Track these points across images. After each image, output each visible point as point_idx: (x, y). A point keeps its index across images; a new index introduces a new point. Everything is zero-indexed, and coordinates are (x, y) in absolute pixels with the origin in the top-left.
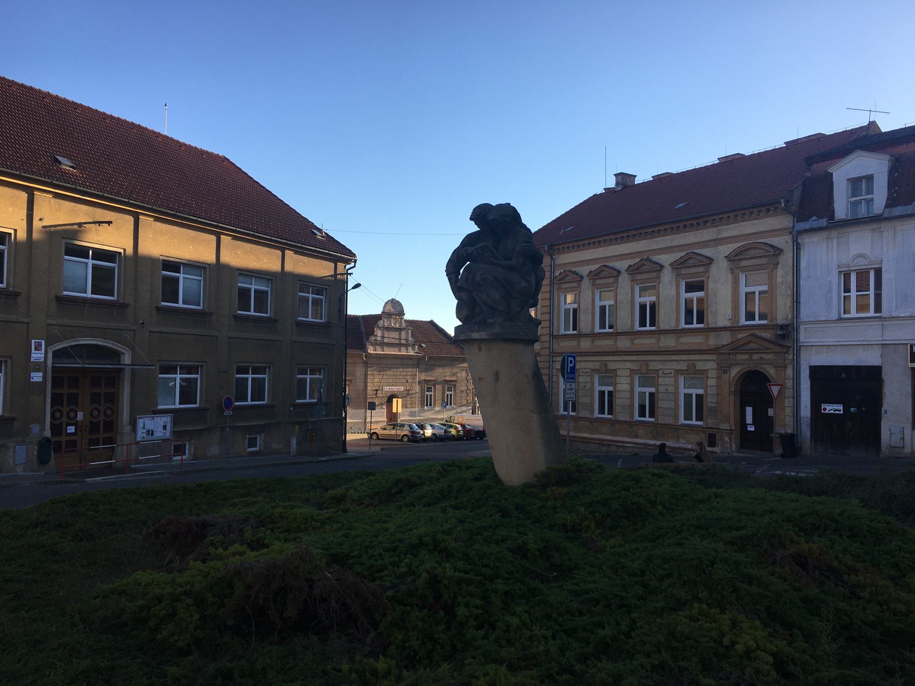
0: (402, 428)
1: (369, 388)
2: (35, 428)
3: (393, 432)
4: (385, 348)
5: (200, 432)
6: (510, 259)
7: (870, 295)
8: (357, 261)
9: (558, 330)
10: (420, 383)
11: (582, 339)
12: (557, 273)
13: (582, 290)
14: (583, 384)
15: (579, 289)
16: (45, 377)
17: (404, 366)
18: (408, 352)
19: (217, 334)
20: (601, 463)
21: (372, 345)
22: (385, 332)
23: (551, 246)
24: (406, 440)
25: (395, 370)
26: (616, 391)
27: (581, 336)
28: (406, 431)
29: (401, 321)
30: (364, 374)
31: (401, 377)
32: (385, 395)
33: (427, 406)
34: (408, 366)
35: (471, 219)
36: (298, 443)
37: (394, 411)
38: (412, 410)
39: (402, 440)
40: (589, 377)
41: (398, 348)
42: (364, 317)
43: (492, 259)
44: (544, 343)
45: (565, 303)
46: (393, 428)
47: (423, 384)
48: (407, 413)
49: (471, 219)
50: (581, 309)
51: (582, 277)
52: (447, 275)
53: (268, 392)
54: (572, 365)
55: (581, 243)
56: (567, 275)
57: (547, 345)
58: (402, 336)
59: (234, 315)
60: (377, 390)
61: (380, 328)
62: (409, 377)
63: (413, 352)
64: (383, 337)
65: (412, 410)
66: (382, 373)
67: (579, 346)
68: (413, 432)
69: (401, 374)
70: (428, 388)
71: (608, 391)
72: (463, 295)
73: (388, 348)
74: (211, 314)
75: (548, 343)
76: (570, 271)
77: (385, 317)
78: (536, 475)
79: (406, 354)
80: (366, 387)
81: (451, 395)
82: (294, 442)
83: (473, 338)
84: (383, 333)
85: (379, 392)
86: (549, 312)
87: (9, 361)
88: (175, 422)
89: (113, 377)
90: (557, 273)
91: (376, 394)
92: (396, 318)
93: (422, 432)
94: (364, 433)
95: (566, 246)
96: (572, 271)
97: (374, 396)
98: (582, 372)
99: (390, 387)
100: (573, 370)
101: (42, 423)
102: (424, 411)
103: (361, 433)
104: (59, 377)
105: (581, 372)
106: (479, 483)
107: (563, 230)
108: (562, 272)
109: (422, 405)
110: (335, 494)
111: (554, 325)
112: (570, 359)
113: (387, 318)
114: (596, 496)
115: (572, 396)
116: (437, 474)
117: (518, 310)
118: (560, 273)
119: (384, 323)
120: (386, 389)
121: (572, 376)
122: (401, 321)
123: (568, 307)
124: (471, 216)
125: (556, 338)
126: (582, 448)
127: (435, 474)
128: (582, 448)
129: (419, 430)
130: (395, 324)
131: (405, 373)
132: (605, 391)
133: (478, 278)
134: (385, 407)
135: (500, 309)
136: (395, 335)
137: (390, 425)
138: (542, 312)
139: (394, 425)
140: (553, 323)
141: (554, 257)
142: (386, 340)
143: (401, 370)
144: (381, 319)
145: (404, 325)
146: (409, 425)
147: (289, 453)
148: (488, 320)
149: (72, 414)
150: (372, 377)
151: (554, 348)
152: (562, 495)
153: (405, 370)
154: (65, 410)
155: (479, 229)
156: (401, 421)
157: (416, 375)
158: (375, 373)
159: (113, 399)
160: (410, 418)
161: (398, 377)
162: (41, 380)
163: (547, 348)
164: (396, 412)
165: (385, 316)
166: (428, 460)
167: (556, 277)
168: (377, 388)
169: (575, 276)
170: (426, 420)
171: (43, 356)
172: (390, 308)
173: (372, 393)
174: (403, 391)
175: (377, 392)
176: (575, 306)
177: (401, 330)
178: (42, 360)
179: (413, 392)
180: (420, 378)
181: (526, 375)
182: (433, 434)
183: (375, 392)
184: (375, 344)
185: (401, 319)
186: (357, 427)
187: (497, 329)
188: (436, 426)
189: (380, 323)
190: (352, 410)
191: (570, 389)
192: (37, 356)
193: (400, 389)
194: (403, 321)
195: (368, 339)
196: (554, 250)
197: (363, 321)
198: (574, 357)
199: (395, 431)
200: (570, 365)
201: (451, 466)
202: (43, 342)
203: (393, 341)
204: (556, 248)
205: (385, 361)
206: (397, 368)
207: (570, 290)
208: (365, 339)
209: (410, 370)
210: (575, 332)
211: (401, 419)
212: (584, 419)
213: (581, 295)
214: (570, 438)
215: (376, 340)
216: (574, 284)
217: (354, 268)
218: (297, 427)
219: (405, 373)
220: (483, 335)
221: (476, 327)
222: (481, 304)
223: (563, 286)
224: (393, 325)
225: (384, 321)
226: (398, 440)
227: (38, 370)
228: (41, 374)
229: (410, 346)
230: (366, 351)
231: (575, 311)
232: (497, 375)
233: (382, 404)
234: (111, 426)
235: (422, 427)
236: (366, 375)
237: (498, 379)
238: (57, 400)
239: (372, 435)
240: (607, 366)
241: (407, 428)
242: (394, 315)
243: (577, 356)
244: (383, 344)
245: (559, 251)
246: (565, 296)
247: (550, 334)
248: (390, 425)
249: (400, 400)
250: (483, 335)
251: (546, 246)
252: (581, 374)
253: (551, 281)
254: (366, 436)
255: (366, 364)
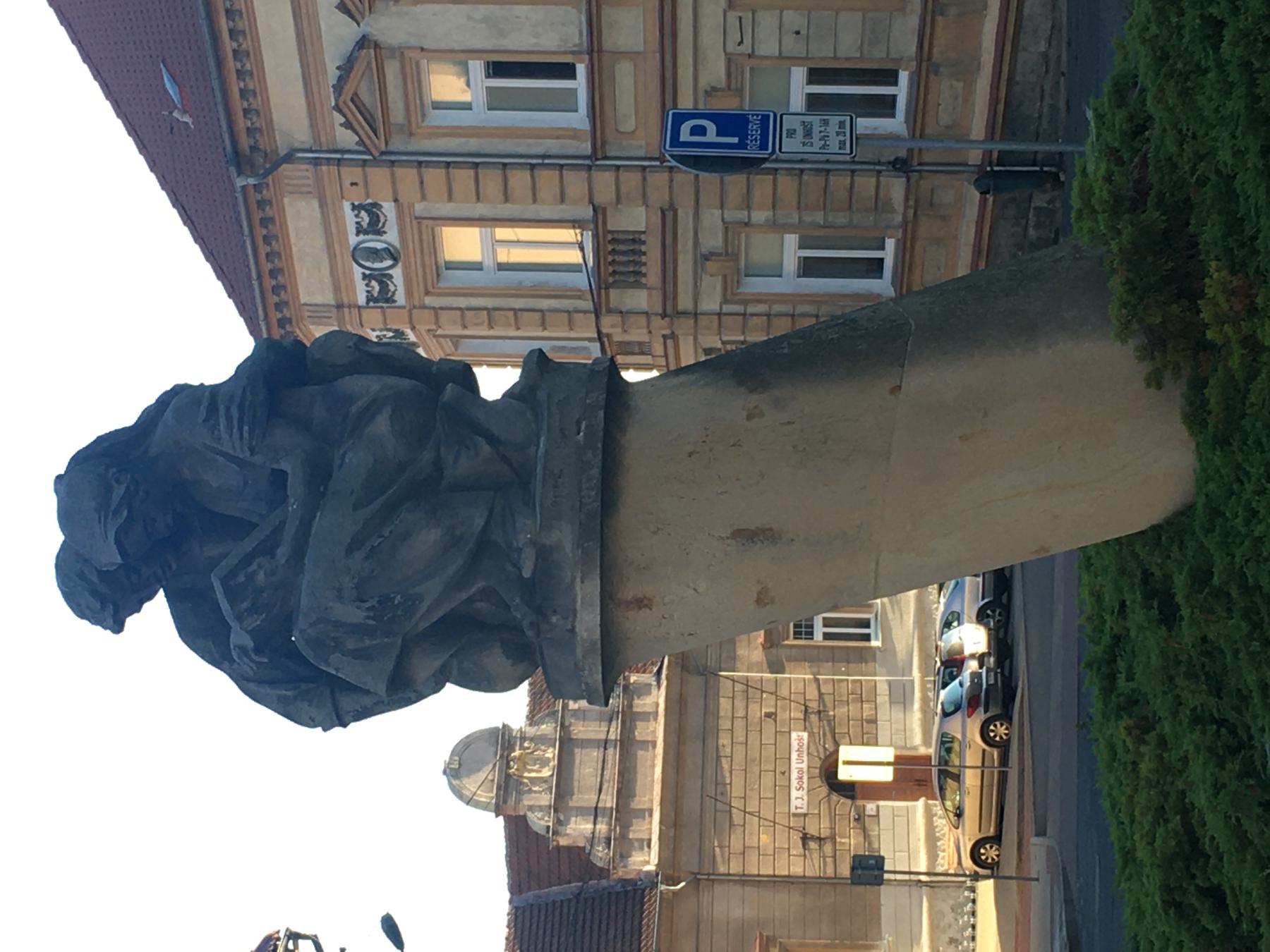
0: (956, 746)
1: (797, 870)
3: (971, 779)
4: (638, 803)
6: (279, 478)
8: (294, 929)
9: (574, 134)
10: (776, 667)
11: (607, 44)
12: (346, 138)
13: (413, 42)
14: (789, 40)
15: (409, 54)
17: (708, 732)
18: (649, 841)
20: (1106, 87)
21: (624, 856)
22: (571, 804)
23: (240, 161)
24: (1002, 730)
25: (726, 766)
26: (807, 58)
27: (594, 48)
28: (969, 730)
29: (532, 739)
30: (737, 889)
31: (754, 739)
32: (824, 807)
33: (867, 638)
34: (710, 713)
35: (118, 627)
38: (883, 698)
39: (1004, 747)
40: (759, 15)
41: (640, 753)
42: (517, 886)
43: (279, 552)
44: (623, 189)
45: (467, 107)
46: (957, 778)
47: (783, 653)
48: (897, 714)
49: (118, 627)
50: (488, 45)
51: (363, 42)
52: (345, 725)
54: (711, 128)
55: (228, 45)
56: (355, 99)
57: (631, 180)
58: (593, 736)
60: (805, 838)
61: (559, 822)
62: (754, 707)
63: (654, 691)
64: (596, 812)
65: (883, 698)
66: (737, 817)
67: (637, 53)
68: (973, 702)
69: (742, 739)
70: (797, 635)
71: (810, 82)
72: (424, 667)
73: (638, 790)
75: (624, 175)
76: (339, 88)
77: (518, 801)
78: (1154, 380)
79: (661, 719)
80: (789, 881)
81: (827, 623)
83: (597, 635)
84: (582, 811)
85: (812, 830)
86: (499, 172)
90: (346, 138)
91: (820, 839)
92: (519, 758)
93: (973, 665)
94: (973, 890)
95: (238, 104)
96: (340, 78)
97: (828, 848)
98: (741, 43)
99: (794, 783)
100: (731, 123)
102: (889, 648)
103: (974, 901)
105: (741, 49)
106: (1185, 612)
107: (175, 114)
108: (343, 120)
109: (864, 657)
111: (554, 151)
112: (685, 135)
113: (520, 793)
114: (1239, 154)
115: (833, 127)
116: (1144, 742)
117: (486, 449)
118: (348, 125)
119: (541, 808)
120: (799, 799)
121: (754, 129)
122: (532, 739)
123: (482, 98)
124: (105, 628)
125: (604, 144)
126: (1042, 47)
127: (1143, 749)
128: (1042, 47)
129: (966, 676)
130: (544, 762)
131: (739, 724)
132: (809, 95)
133: (353, 614)
134: (870, 807)
135: (480, 522)
136: (587, 766)
137: (942, 789)
138: (501, 197)
139: (944, 774)
140: (544, 157)
141: (282, 152)
142: (609, 801)
143: (724, 740)
144: (525, 817)
145: (547, 728)
146: (946, 714)
148: (527, 574)
150: (753, 857)
151: (641, 153)
152: (1236, 282)
153: (725, 724)
155: (161, 593)
156: (926, 742)
157: (747, 683)
158: (736, 843)
160: (917, 705)
161: (754, 753)
163: (644, 179)
164: (891, 769)
165: (512, 801)
166: (1082, 726)
167: (361, 142)
168: (796, 837)
169: (359, 68)
170: (923, 639)
172: (481, 782)
173: (816, 855)
174: (811, 735)
175: (813, 838)
176: (477, 67)
177: (570, 739)
179: (812, 694)
180: (759, 664)
181: (750, 417)
182: (981, 617)
183: (813, 845)
184: (623, 843)
185: (523, 739)
186: (950, 917)
187: (564, 537)
188: (947, 605)
189: (540, 821)
190: (881, 939)
191: (808, 133)
193: (801, 747)
194: (531, 731)
195: (603, 873)
196: (254, 148)
197: (529, 889)
198: (680, 119)
199: (968, 772)
200: (712, 135)
201: (1112, 678)
203: (612, 771)
204: (245, 142)
205: (691, 803)
206: (718, 757)
207: (414, 83)
208: (604, 882)
209: (724, 703)
210: (581, 69)
211: (917, 739)
212: (924, 37)
213: (433, 47)
214: (997, 137)
215: (608, 840)
216: (392, 70)
217: (321, 941)
219: (739, 724)
220: (587, 591)
221: (554, 619)
222: (464, 596)
223: (397, 115)
224: (546, 773)
225: (531, 808)
226: (1004, 760)
229: (630, 706)
230: (651, 881)
231: (498, 69)
232: (748, 536)
233: (860, 818)
235: (953, 664)
236: (745, 880)
237: (764, 531)
239: (990, 868)
240: (714, 89)
241: (954, 726)
242: (508, 767)
243: (675, 106)
244: (624, 812)
245: (260, 130)
246: (438, 106)
247: (589, 168)
248: (942, 789)
249: (846, 752)
250: (587, 591)
251: (240, 182)
252: (746, 48)
253: (376, 162)
254: (986, 889)
255: (703, 879)
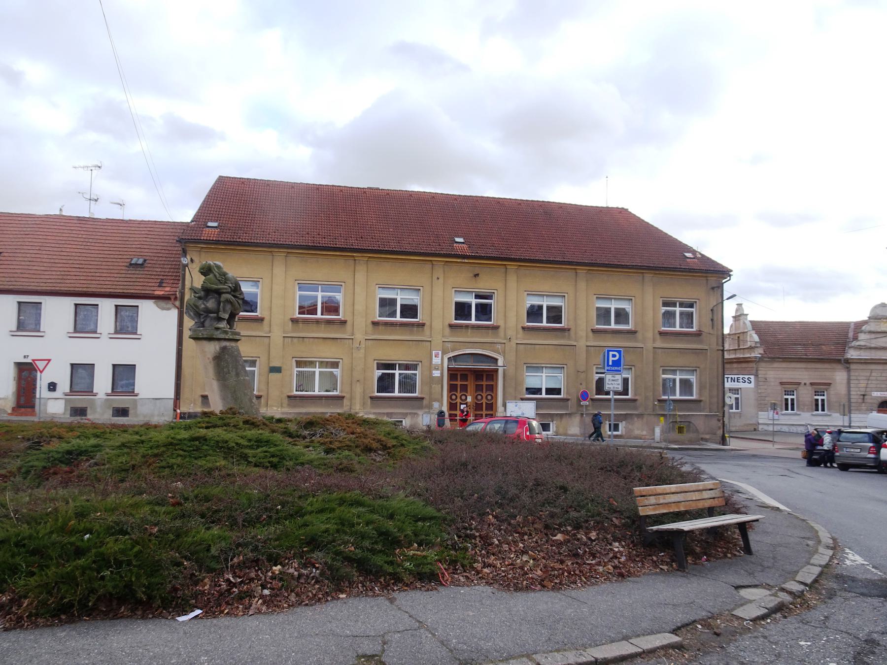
2: (436, 405)
5: (561, 415)
7: (43, 304)
16: (442, 374)
19: (575, 343)
36: (662, 432)
37: (470, 397)
53: (631, 388)
59: (592, 329)
60: (864, 395)
74: (569, 330)
82: (658, 431)
87: (420, 364)
88: (537, 407)
89: (492, 375)
101: (441, 401)
104: (453, 374)
110: (252, 434)
147: (654, 439)
149: (463, 397)
154: (459, 395)
159: (492, 388)
162: (439, 375)
171: (440, 360)
178: (440, 363)
192: (436, 361)
202: (440, 352)
218: (662, 419)
227: (437, 369)
228: (439, 372)
234: (491, 407)
238: (452, 388)
